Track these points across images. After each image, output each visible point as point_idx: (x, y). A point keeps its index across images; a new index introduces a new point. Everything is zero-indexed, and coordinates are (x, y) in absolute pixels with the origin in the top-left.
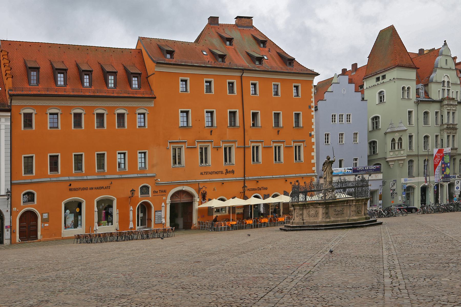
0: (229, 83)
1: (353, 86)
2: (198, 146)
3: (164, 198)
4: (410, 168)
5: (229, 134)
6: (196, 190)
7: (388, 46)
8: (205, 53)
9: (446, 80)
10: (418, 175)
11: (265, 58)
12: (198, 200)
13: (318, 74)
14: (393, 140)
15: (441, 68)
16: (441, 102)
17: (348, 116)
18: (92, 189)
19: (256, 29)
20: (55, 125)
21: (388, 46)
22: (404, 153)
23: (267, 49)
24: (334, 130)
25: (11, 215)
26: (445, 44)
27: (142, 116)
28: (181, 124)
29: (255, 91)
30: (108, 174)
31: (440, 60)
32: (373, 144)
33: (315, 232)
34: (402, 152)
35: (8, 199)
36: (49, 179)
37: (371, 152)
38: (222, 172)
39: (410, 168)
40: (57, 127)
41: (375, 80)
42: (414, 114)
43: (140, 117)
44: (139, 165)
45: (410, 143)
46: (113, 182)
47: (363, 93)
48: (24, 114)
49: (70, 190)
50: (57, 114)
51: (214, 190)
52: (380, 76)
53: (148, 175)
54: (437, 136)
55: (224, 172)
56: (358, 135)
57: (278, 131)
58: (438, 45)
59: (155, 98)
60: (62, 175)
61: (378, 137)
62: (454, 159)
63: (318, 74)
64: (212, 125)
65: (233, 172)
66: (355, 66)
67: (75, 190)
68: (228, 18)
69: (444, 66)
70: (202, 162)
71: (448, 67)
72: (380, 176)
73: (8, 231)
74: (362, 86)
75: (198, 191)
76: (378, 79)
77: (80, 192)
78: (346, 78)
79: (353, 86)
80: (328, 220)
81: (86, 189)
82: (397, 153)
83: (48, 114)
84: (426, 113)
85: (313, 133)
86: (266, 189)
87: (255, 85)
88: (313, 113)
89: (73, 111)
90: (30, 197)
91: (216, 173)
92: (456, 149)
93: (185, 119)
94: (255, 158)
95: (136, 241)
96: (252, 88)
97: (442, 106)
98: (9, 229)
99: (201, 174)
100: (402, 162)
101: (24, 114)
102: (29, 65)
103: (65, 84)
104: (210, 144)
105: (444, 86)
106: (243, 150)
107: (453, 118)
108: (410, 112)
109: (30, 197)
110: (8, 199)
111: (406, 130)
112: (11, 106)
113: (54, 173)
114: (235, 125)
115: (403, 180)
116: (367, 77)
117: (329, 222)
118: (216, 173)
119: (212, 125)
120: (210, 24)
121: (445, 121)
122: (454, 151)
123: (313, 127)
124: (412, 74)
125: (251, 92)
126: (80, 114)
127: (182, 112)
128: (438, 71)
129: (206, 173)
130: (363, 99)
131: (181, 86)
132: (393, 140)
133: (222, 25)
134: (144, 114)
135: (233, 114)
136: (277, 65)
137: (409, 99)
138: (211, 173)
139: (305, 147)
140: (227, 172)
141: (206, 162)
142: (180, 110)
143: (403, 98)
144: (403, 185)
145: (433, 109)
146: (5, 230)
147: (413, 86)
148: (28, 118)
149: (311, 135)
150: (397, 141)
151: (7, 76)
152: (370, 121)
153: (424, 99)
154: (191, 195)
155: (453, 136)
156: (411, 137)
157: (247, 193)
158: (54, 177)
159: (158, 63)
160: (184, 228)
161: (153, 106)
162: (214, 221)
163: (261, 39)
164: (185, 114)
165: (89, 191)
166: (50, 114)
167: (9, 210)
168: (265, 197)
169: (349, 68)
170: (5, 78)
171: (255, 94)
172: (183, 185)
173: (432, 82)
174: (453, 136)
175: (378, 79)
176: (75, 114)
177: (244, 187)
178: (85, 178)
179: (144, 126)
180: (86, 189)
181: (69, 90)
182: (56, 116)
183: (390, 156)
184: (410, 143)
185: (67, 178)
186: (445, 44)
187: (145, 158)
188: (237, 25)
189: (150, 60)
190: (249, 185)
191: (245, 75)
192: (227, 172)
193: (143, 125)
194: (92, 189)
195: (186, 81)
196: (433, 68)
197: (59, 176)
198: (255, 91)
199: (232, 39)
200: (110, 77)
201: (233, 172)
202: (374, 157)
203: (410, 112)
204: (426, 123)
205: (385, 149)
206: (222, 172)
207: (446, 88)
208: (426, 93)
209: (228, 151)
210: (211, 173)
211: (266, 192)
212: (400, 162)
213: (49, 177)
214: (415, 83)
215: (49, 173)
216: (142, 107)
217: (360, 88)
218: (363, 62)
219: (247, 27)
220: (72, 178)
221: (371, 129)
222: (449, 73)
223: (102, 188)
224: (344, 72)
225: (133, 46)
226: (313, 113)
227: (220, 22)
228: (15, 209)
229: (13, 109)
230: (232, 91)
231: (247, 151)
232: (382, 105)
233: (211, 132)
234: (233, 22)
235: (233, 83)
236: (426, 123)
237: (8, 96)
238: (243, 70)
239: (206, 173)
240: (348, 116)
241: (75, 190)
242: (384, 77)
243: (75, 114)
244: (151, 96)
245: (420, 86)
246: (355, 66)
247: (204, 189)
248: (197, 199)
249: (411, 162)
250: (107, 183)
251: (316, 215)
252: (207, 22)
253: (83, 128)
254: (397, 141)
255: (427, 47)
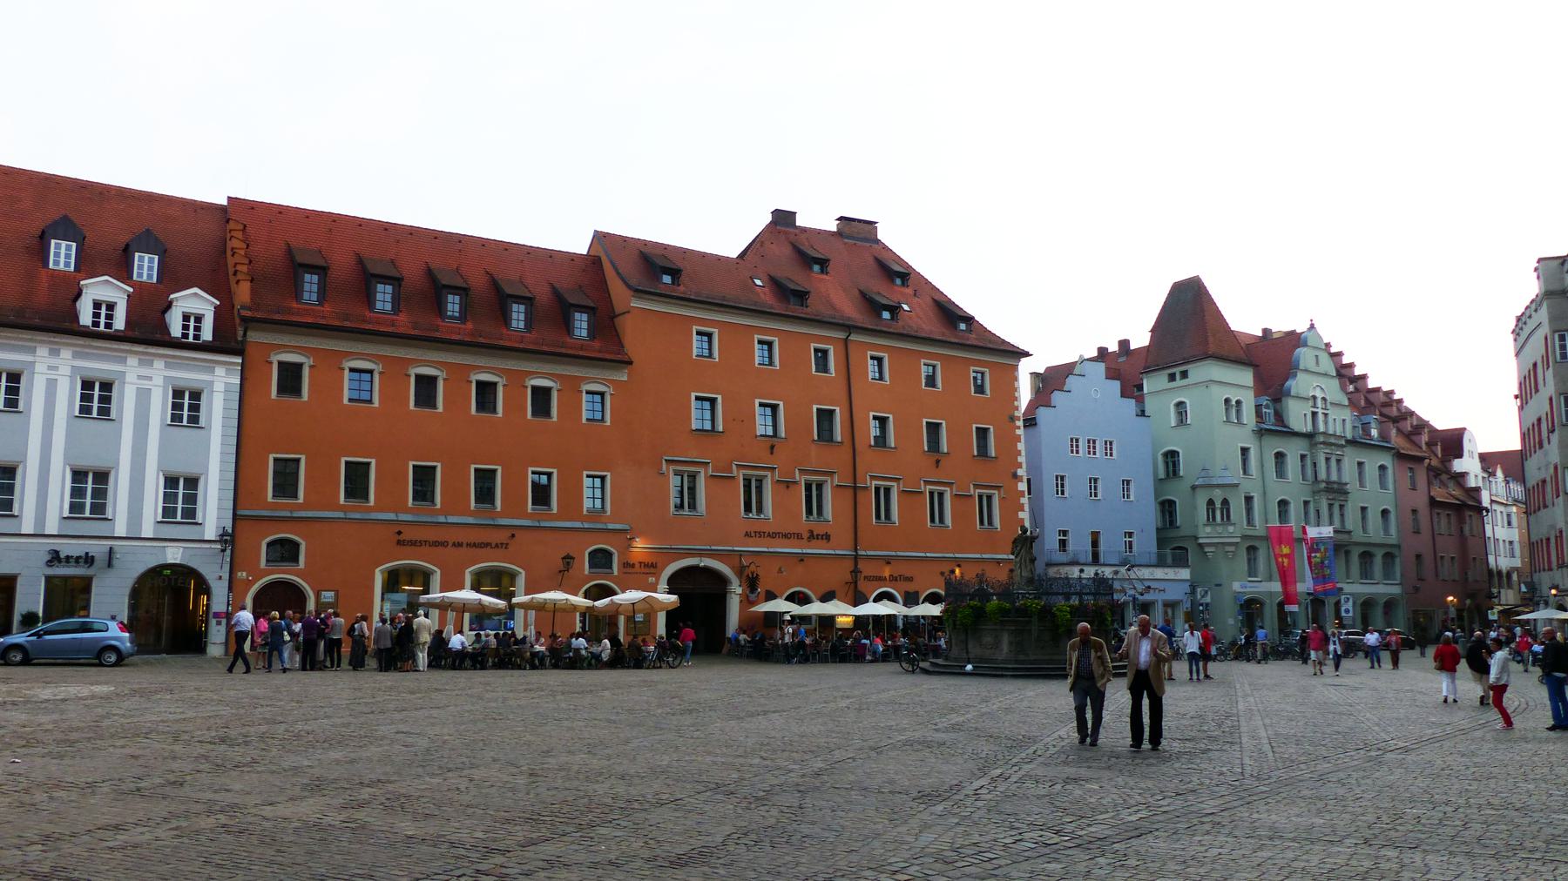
0: (816, 350)
1: (1117, 384)
2: (802, 480)
3: (652, 580)
4: (1252, 561)
5: (817, 456)
6: (733, 568)
7: (1189, 318)
8: (758, 282)
9: (1319, 394)
10: (1270, 579)
11: (906, 307)
12: (739, 590)
13: (1027, 354)
14: (1211, 503)
15: (1306, 371)
16: (1309, 436)
17: (1109, 445)
18: (460, 545)
19: (885, 248)
20: (365, 396)
21: (1189, 318)
22: (1236, 529)
23: (909, 291)
24: (1078, 470)
25: (230, 589)
26: (1312, 326)
27: (597, 398)
28: (760, 431)
29: (881, 372)
30: (503, 514)
31: (1305, 356)
32: (1167, 508)
33: (994, 681)
34: (1231, 529)
35: (223, 551)
36: (341, 515)
37: (1164, 521)
38: (799, 536)
39: (1252, 561)
40: (370, 401)
41: (1166, 378)
42: (1253, 454)
43: (592, 397)
44: (587, 504)
45: (1249, 510)
46: (518, 534)
47: (1140, 400)
48: (280, 363)
49: (399, 543)
50: (371, 372)
51: (780, 571)
52: (1177, 370)
53: (611, 526)
54: (1306, 503)
55: (806, 535)
56: (1132, 485)
57: (938, 462)
58: (1301, 327)
59: (631, 363)
60: (377, 509)
61: (1178, 492)
62: (1347, 553)
63: (1027, 354)
64: (775, 434)
65: (827, 537)
66: (1124, 344)
67: (413, 543)
68: (818, 216)
69: (1312, 366)
70: (748, 508)
71: (1321, 369)
72: (1185, 574)
73: (219, 623)
74: (1140, 387)
75: (740, 571)
76: (1172, 377)
77: (425, 549)
78: (1101, 367)
79: (1117, 384)
80: (1022, 657)
81: (444, 544)
82: (1220, 529)
83: (347, 372)
84: (1280, 456)
85: (1020, 472)
86: (910, 579)
87: (880, 360)
88: (1018, 432)
89: (414, 371)
90: (285, 551)
91: (786, 536)
92: (1349, 532)
93: (769, 421)
94: (882, 511)
95: (375, 683)
96: (872, 367)
97: (1313, 445)
98: (224, 621)
99: (747, 534)
100: (1232, 549)
101: (280, 363)
102: (299, 259)
103: (396, 307)
104: (769, 474)
105: (1315, 406)
106: (851, 492)
107: (1339, 470)
108: (1245, 451)
109: (285, 551)
110: (223, 551)
111: (1236, 485)
112: (244, 342)
113: (353, 503)
114: (831, 439)
115: (1236, 586)
116: (1150, 369)
117: (1022, 662)
118: (786, 536)
119: (775, 434)
120: (773, 223)
121: (1322, 475)
122: (1345, 537)
123: (1022, 459)
124: (1246, 377)
125: (871, 375)
126: (548, 391)
127: (761, 405)
128: (1300, 376)
129: (760, 534)
130: (1142, 413)
131: (759, 353)
132: (1211, 503)
133: (804, 230)
134: (602, 394)
135: (826, 416)
136: (929, 324)
137: (1240, 423)
138: (772, 535)
139: (1002, 499)
140: (812, 536)
141: (760, 510)
142: (693, 395)
143: (1228, 421)
144: (1237, 595)
145: (1293, 450)
146: (213, 622)
147: (1249, 400)
148: (290, 378)
149: (1015, 476)
150: (1218, 505)
151: (239, 276)
152: (1160, 459)
153: (1273, 426)
154: (722, 581)
155: (1341, 507)
156: (1249, 499)
157: (863, 586)
158: (354, 509)
159: (637, 291)
160: (696, 652)
161: (625, 378)
162: (764, 644)
163: (897, 268)
164: (768, 411)
165: (450, 549)
166: (352, 370)
167: (226, 576)
168: (911, 599)
169: (1113, 347)
170: (232, 280)
171: (881, 378)
172: (701, 555)
173: (1288, 394)
174: (1341, 507)
175: (1172, 377)
176: (418, 377)
177: (856, 572)
178: (442, 519)
179: (603, 420)
180: (444, 544)
181: (403, 322)
182: (366, 377)
183: (1206, 533)
184: (1249, 510)
185: (391, 516)
186: (1312, 326)
187: (603, 488)
188: (839, 234)
189: (620, 283)
190: (867, 569)
191: (852, 337)
192: (812, 536)
193: (598, 416)
194: (460, 545)
195: (710, 335)
196: (1291, 369)
197: (370, 509)
198: (881, 372)
199: (828, 260)
200: (450, 297)
201: (827, 537)
202: (1172, 533)
203: (1245, 451)
204: (1281, 473)
205: (1193, 516)
206: (799, 536)
207: (1320, 411)
208: (1279, 417)
209: (814, 493)
210: (772, 535)
211: (911, 587)
212: (1228, 548)
213: (471, 514)
214: (1251, 394)
215: (270, 499)
216: (595, 380)
217: (1132, 390)
218: (1140, 339)
219: (866, 240)
220: (403, 517)
221: (1162, 474)
222: (1323, 382)
223: (487, 545)
224: (1103, 353)
225: (582, 249)
226: (1018, 432)
227: (800, 222)
228: (242, 575)
229: (250, 350)
230: (822, 365)
231: (860, 495)
232: (1182, 430)
233: (772, 447)
234: (833, 227)
235: (825, 352)
236: (1281, 473)
237: (237, 321)
238: (850, 328)
239: (760, 534)
240: (1109, 445)
241: (413, 543)
242: (1184, 375)
243: (418, 377)
244: (619, 357)
245: (1264, 401)
246: (1124, 344)
247: (753, 568)
248: (736, 589)
249: (1252, 550)
250: (502, 536)
251: (997, 645)
252: (769, 219)
253: (440, 408)
254: (1218, 505)
255: (1280, 326)
